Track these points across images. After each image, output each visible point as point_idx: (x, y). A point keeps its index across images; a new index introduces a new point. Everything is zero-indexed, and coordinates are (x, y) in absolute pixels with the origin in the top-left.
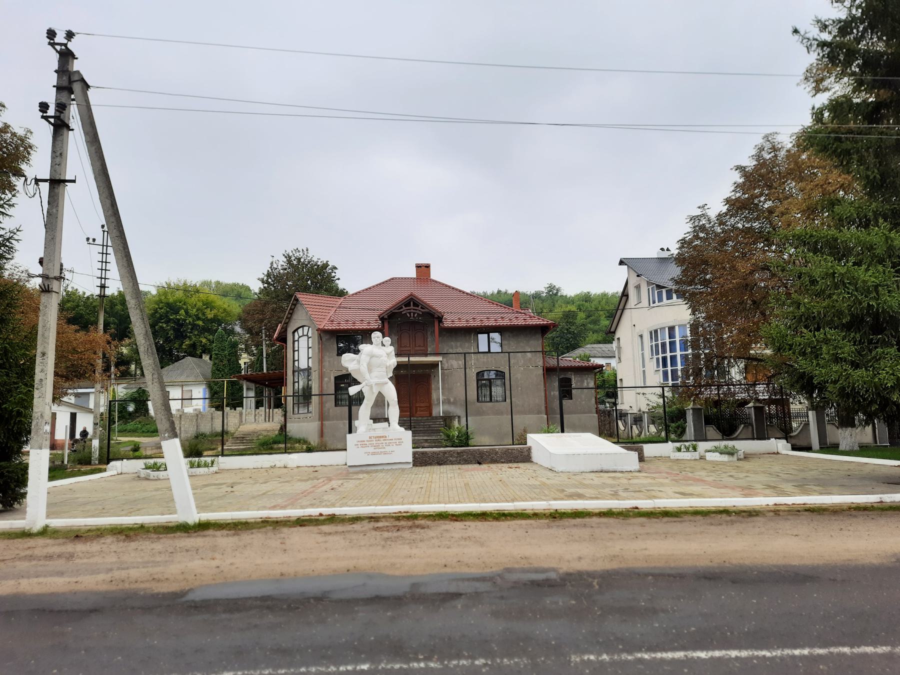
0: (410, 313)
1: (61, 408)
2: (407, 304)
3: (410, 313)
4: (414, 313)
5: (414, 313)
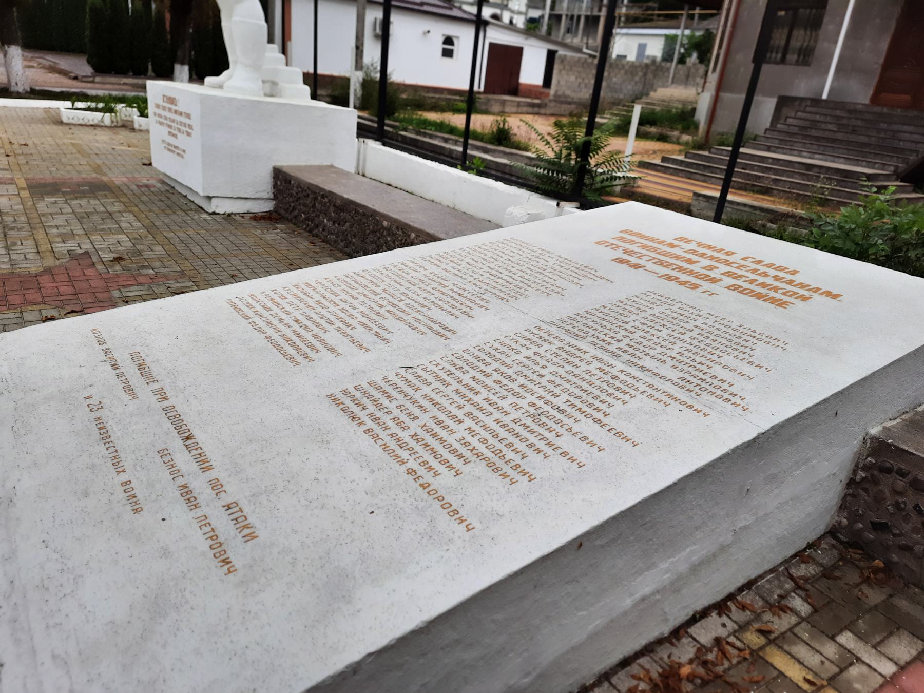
1: (533, 42)
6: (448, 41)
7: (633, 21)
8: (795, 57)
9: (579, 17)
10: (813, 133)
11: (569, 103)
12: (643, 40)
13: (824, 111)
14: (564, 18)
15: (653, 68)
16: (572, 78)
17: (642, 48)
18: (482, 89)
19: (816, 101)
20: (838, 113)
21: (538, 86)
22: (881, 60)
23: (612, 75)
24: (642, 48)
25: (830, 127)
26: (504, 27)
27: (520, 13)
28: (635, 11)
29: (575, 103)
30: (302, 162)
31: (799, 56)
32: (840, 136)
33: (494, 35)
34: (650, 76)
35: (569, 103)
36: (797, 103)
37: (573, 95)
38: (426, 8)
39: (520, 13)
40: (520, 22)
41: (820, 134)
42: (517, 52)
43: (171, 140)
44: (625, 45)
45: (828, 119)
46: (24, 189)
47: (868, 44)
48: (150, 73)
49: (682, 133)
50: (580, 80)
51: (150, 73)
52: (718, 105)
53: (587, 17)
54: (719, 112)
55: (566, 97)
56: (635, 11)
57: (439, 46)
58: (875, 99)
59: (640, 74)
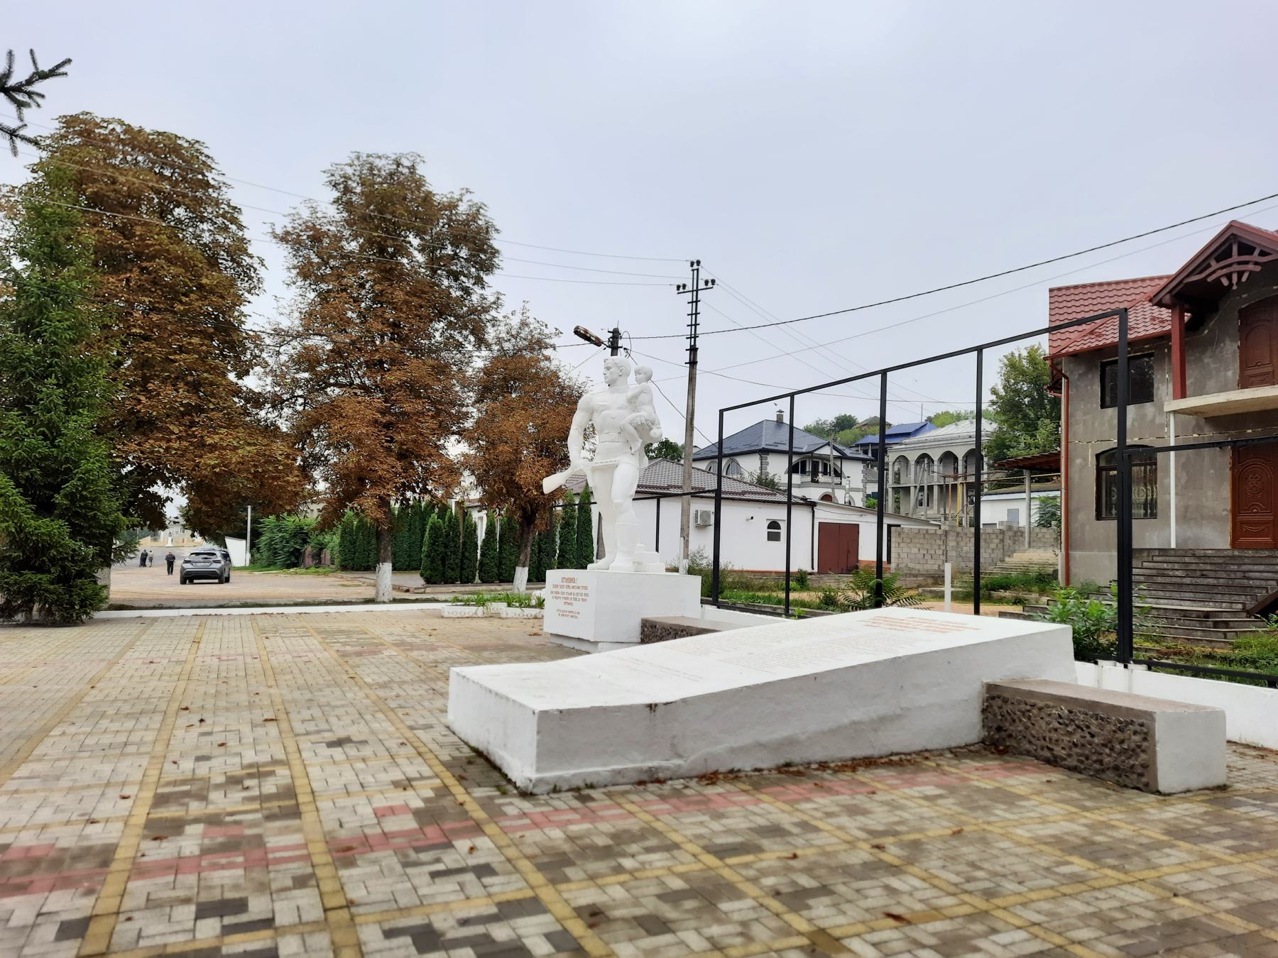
0: (1229, 276)
3: (1229, 276)
4: (1240, 274)
5: (1240, 274)
6: (774, 525)
7: (999, 486)
8: (1142, 511)
9: (931, 488)
10: (1160, 580)
11: (916, 576)
12: (1013, 506)
13: (1172, 559)
14: (912, 489)
15: (1010, 533)
16: (915, 550)
17: (1013, 513)
18: (816, 570)
19: (1164, 552)
20: (1187, 560)
21: (1224, 730)
22: (1229, 507)
23: (962, 544)
24: (1013, 513)
25: (1178, 573)
26: (839, 507)
27: (857, 490)
28: (1000, 475)
29: (923, 575)
30: (671, 615)
31: (1145, 509)
32: (1187, 581)
33: (826, 515)
34: (1007, 542)
35: (916, 576)
36: (1145, 554)
37: (918, 567)
38: (747, 496)
39: (857, 490)
40: (859, 501)
41: (1167, 580)
42: (855, 528)
43: (569, 608)
44: (994, 511)
45: (1176, 566)
46: (1124, 328)
47: (1210, 493)
48: (477, 580)
49: (1041, 595)
50: (923, 552)
51: (477, 580)
52: (1072, 563)
53: (940, 486)
54: (1073, 570)
55: (910, 569)
56: (1000, 475)
57: (765, 531)
58: (1234, 544)
59: (997, 541)
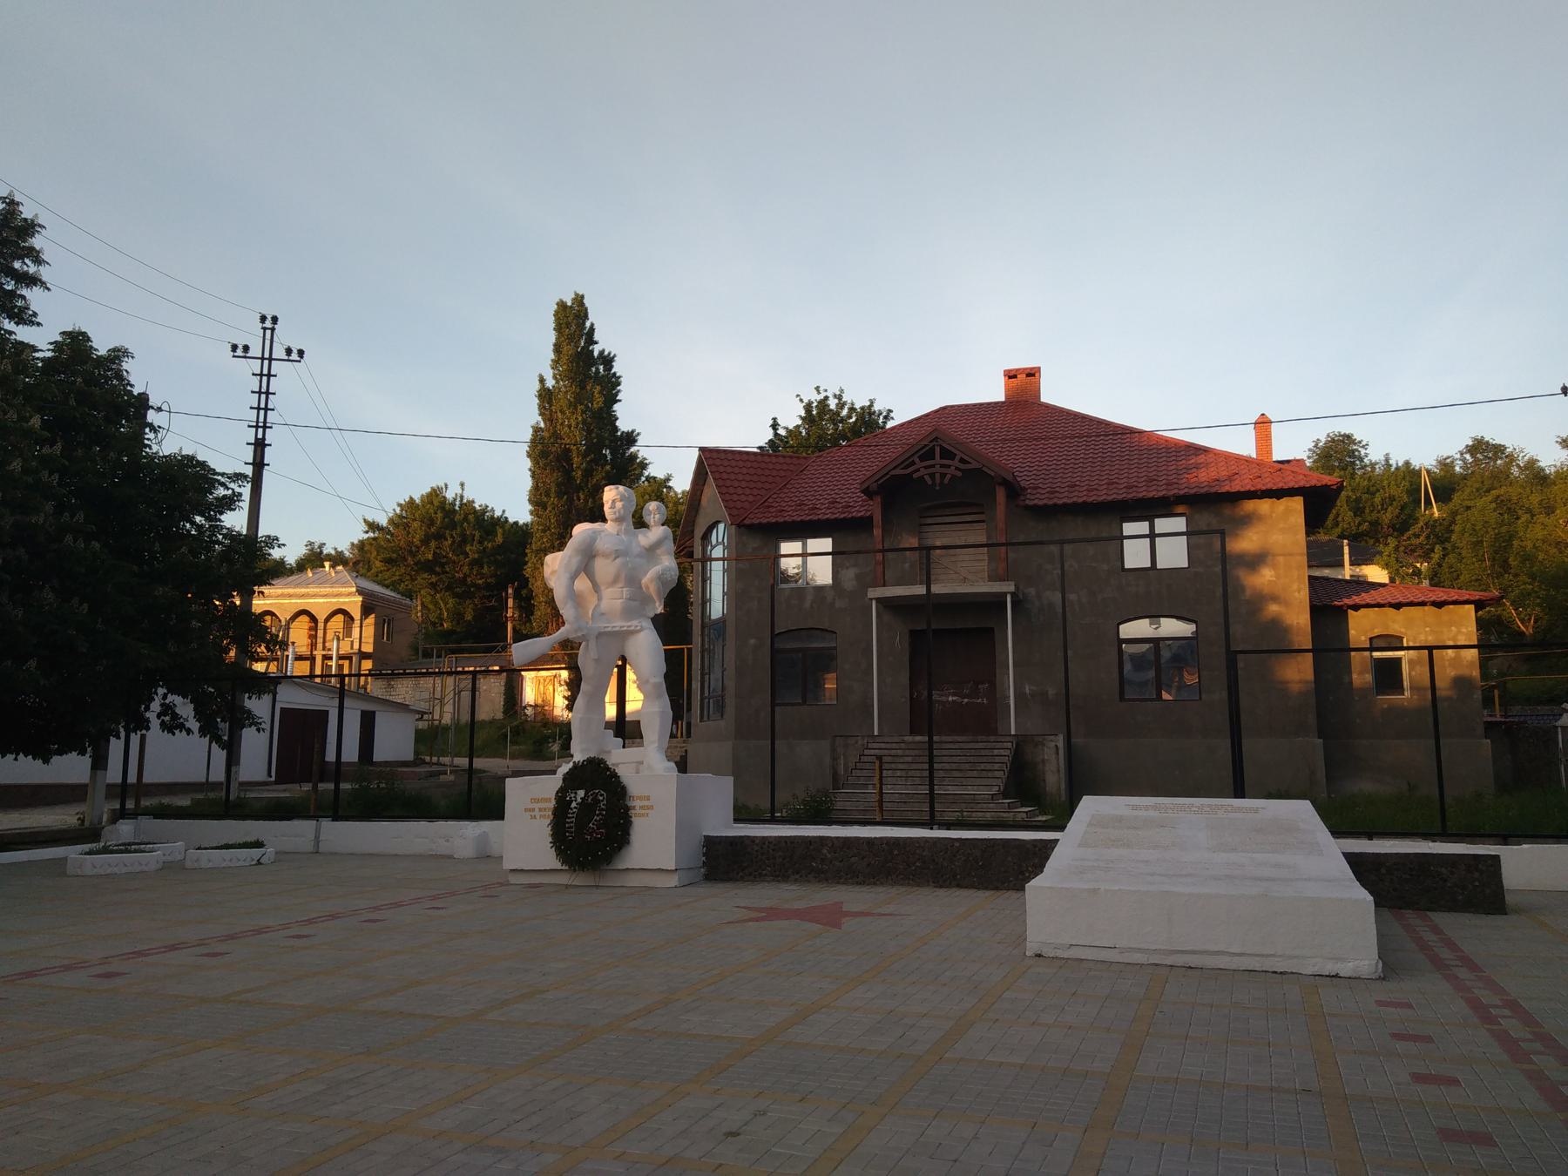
0: (932, 476)
2: (928, 455)
